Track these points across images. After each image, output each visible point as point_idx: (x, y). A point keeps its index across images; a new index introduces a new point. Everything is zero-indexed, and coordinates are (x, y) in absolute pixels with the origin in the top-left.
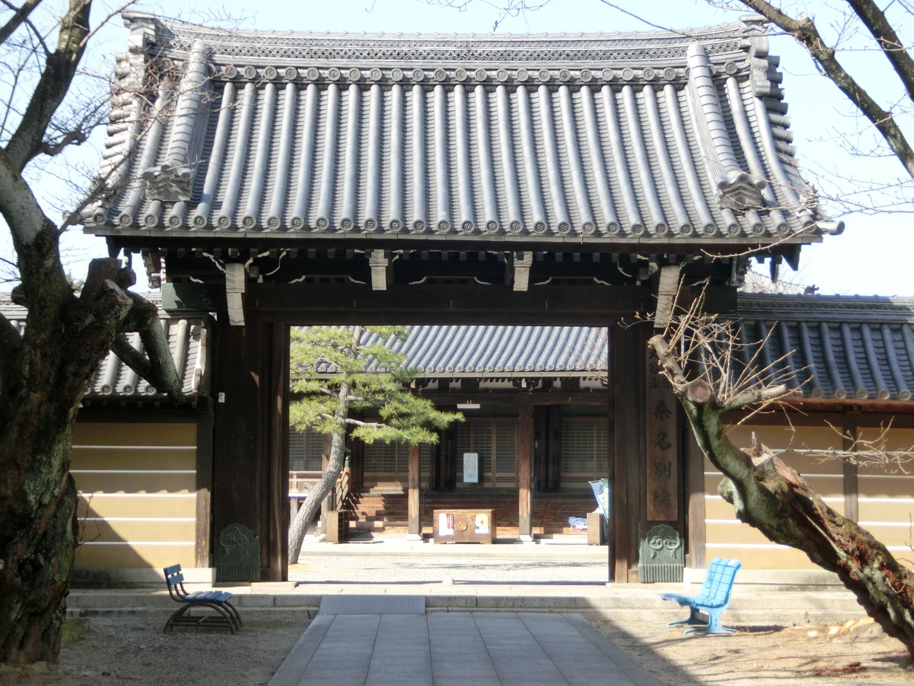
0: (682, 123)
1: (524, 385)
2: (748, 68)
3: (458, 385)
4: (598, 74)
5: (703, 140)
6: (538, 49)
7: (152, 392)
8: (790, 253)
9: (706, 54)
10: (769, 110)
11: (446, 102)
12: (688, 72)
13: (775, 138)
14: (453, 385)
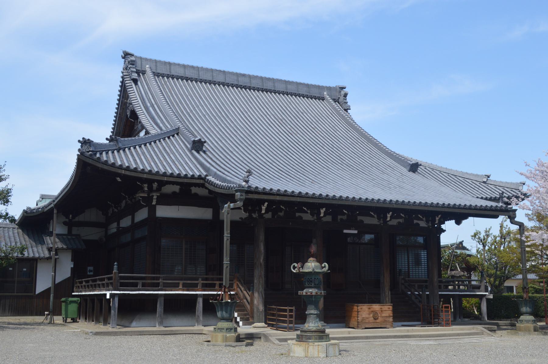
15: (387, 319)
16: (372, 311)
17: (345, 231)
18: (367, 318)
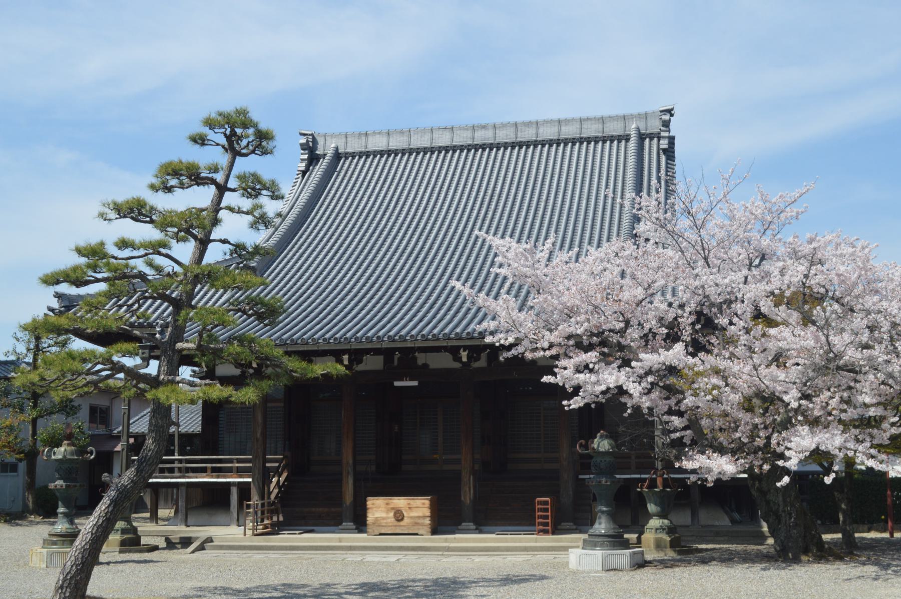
15: (421, 521)
16: (393, 509)
17: (397, 384)
18: (384, 518)
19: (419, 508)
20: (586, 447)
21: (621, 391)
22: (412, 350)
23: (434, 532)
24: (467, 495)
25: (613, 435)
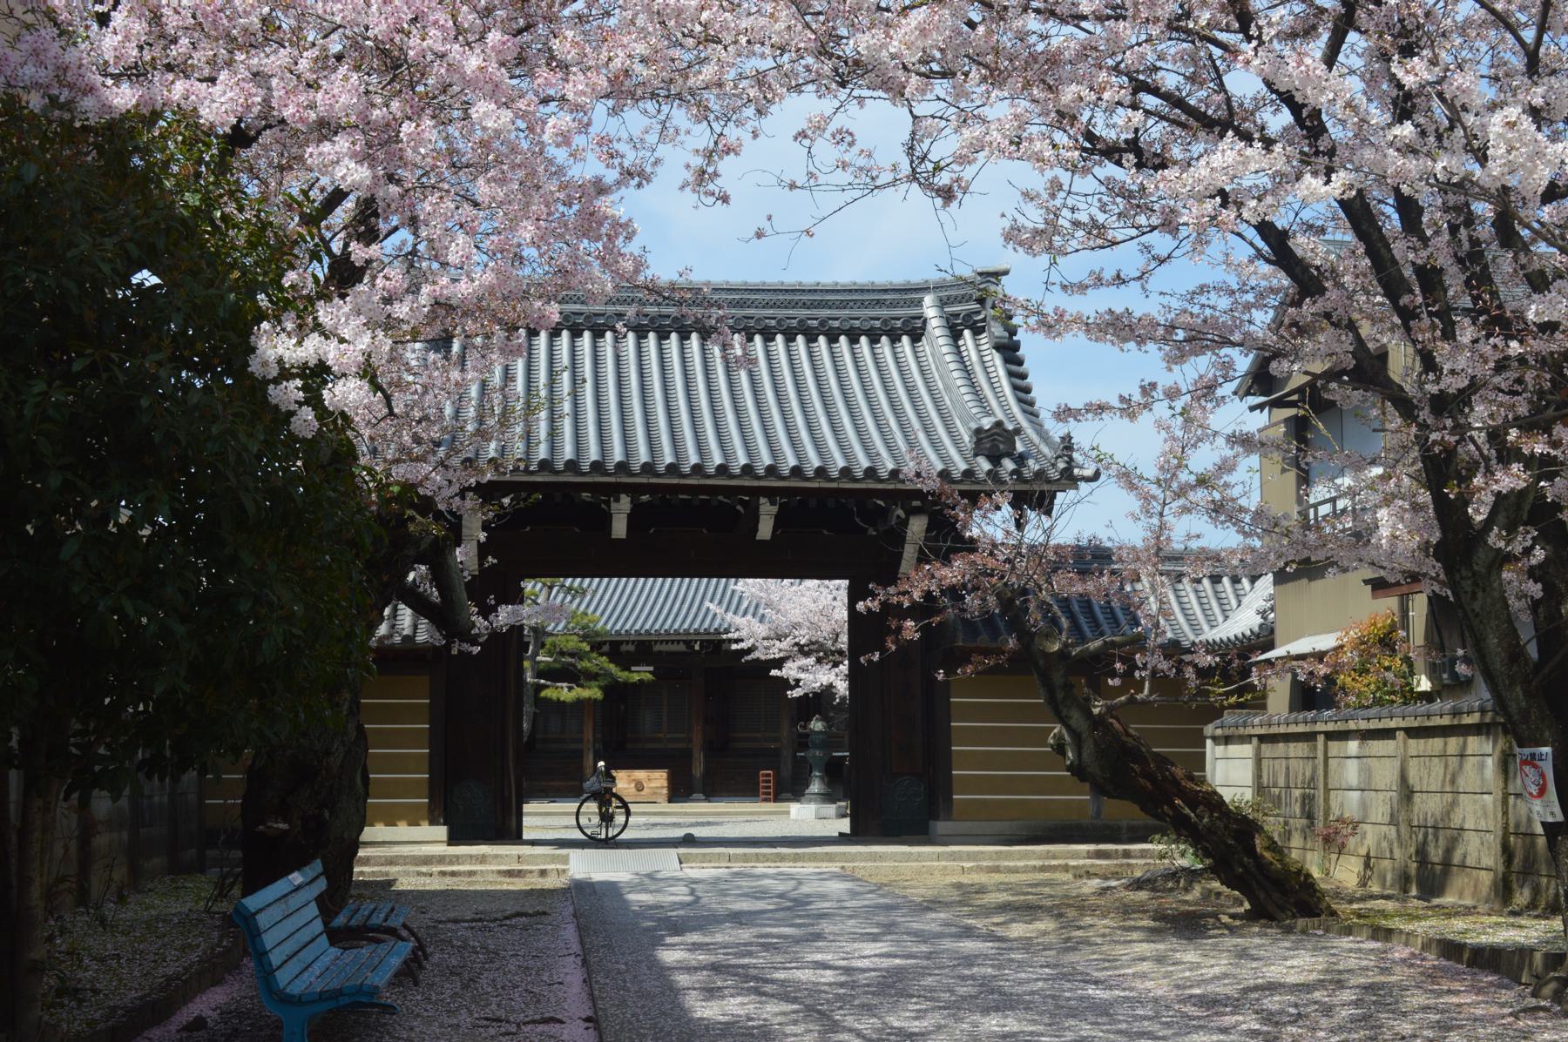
0: (922, 372)
1: (697, 647)
2: (984, 320)
3: (631, 648)
4: (857, 323)
5: (947, 388)
6: (774, 298)
7: (440, 641)
8: (1044, 503)
9: (942, 303)
10: (1007, 361)
11: (595, 348)
12: (925, 321)
13: (1015, 388)
14: (624, 648)
19: (657, 779)
20: (805, 727)
21: (831, 686)
22: (621, 642)
23: (670, 801)
24: (698, 770)
25: (825, 718)
